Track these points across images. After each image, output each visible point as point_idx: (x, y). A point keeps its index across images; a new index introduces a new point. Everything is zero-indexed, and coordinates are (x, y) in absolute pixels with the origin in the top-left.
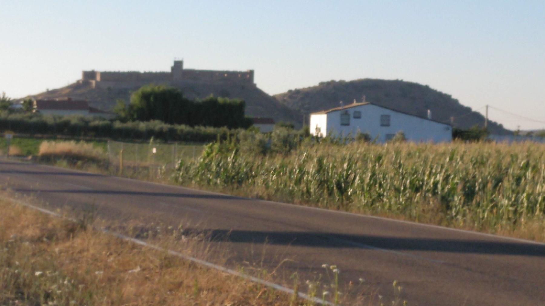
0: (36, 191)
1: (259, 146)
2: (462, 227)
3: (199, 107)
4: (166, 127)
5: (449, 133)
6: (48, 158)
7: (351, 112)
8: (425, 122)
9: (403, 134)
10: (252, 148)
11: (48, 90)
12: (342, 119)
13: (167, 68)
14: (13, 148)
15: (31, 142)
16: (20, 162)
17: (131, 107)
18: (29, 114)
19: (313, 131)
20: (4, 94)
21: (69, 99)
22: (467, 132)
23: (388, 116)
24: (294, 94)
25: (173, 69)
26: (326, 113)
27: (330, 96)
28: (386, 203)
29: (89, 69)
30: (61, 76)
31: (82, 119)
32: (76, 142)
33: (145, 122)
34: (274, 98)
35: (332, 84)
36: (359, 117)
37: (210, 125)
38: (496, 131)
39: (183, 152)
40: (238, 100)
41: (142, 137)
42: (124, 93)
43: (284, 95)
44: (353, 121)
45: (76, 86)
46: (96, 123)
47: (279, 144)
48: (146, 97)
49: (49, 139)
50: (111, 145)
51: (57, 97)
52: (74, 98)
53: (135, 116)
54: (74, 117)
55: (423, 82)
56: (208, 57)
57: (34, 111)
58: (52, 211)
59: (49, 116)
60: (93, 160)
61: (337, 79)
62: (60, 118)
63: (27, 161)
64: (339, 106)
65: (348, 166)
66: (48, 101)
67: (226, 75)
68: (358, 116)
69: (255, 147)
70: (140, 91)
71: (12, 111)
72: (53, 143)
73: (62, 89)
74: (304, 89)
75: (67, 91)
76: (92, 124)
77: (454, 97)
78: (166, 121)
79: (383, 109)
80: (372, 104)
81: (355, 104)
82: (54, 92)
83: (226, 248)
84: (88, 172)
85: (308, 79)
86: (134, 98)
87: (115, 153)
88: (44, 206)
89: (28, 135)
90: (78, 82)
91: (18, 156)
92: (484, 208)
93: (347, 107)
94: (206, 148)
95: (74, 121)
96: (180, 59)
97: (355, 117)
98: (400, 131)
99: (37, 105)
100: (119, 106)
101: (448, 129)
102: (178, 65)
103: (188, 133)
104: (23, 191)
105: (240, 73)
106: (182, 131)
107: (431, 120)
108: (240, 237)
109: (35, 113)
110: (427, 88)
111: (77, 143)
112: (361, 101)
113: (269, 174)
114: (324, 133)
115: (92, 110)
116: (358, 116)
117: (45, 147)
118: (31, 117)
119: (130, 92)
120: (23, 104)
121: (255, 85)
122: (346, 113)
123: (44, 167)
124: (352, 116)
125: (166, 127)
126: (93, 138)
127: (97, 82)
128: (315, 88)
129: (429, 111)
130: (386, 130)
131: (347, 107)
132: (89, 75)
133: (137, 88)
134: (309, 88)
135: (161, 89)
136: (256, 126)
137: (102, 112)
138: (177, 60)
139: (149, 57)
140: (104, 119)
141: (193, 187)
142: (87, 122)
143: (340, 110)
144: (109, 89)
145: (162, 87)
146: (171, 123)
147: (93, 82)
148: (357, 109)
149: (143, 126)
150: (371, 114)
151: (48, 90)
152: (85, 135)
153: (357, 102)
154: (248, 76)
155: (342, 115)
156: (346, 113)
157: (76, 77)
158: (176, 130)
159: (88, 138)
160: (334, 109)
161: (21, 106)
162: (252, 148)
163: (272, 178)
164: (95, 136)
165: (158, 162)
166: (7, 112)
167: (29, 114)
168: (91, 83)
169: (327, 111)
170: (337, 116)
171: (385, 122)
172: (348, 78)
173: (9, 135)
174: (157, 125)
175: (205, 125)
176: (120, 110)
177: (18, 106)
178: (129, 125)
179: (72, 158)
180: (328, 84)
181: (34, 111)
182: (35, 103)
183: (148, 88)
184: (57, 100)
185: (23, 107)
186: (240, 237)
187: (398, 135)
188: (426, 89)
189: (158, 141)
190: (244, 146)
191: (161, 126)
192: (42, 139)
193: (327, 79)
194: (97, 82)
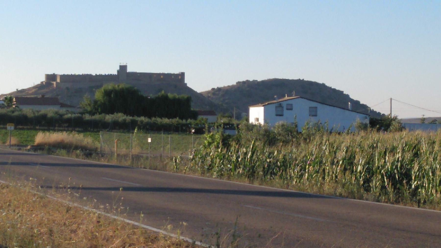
0: (79, 188)
2: (276, 185)
3: (153, 101)
6: (40, 147)
7: (284, 104)
11: (17, 90)
13: (114, 71)
14: (12, 138)
17: (96, 102)
19: (252, 120)
22: (381, 120)
26: (263, 106)
30: (29, 78)
31: (56, 113)
34: (201, 94)
35: (247, 83)
36: (291, 109)
39: (196, 143)
42: (91, 91)
43: (208, 92)
44: (286, 112)
48: (107, 93)
49: (44, 130)
50: (103, 135)
54: (50, 111)
55: (313, 80)
56: (147, 61)
58: (158, 227)
59: (28, 110)
61: (251, 80)
62: (38, 112)
64: (275, 99)
66: (21, 98)
68: (290, 108)
70: (102, 89)
72: (47, 134)
73: (29, 89)
74: (224, 87)
75: (34, 90)
76: (66, 117)
78: (126, 113)
79: (312, 102)
80: (302, 98)
81: (286, 98)
82: (23, 91)
86: (99, 95)
90: (42, 82)
93: (280, 100)
95: (50, 115)
96: (125, 64)
97: (287, 109)
100: (85, 101)
101: (366, 118)
102: (123, 68)
103: (147, 124)
105: (174, 75)
107: (351, 111)
110: (323, 85)
111: (69, 134)
114: (262, 122)
115: (63, 105)
116: (290, 108)
117: (41, 137)
118: (13, 112)
122: (280, 105)
125: (129, 118)
126: (66, 129)
127: (57, 83)
128: (233, 86)
129: (349, 103)
131: (280, 100)
132: (51, 78)
135: (120, 87)
138: (122, 64)
142: (61, 116)
143: (275, 103)
144: (67, 88)
146: (133, 116)
148: (290, 102)
149: (109, 118)
150: (301, 106)
154: (180, 77)
155: (276, 107)
157: (41, 79)
158: (137, 121)
160: (270, 102)
162: (258, 138)
164: (67, 127)
168: (53, 84)
169: (263, 105)
170: (273, 108)
172: (260, 78)
173: (10, 127)
174: (120, 117)
176: (86, 105)
178: (97, 117)
180: (244, 82)
182: (14, 100)
191: (123, 118)
194: (57, 83)
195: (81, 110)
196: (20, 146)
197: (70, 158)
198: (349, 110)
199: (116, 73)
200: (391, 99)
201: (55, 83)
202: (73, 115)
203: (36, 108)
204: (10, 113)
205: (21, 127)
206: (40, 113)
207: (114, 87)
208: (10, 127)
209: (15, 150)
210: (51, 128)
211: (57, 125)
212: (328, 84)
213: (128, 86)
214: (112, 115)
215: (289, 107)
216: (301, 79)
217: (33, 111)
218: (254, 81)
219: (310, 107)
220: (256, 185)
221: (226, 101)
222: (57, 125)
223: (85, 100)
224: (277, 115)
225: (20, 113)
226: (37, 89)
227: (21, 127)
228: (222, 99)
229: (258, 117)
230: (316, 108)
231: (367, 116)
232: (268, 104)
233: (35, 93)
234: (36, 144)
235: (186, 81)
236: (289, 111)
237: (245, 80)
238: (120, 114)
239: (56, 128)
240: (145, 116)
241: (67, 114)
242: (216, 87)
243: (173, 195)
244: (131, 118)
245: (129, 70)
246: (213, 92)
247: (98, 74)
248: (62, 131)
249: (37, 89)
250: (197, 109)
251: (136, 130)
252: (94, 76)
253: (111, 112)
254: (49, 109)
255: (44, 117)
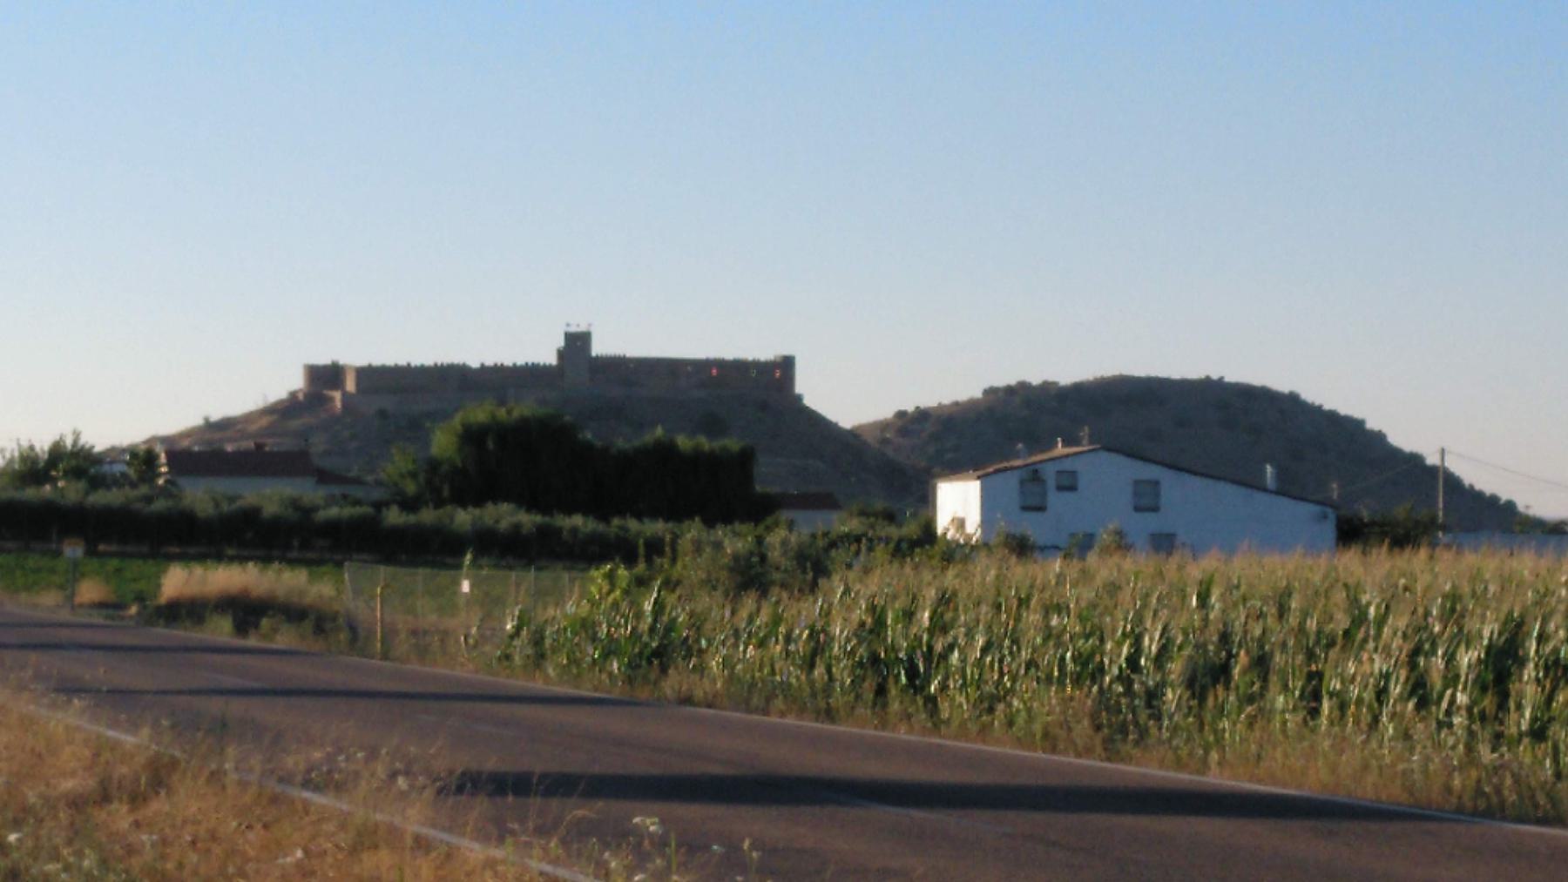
0: (99, 691)
1: (731, 570)
4: (528, 520)
5: (1329, 530)
6: (187, 611)
7: (1049, 473)
8: (1259, 496)
9: (1119, 534)
10: (714, 576)
11: (206, 419)
12: (1022, 493)
15: (135, 567)
16: (101, 621)
17: (433, 466)
18: (144, 490)
19: (943, 522)
20: (77, 435)
21: (259, 447)
23: (1156, 483)
24: (912, 423)
25: (561, 354)
27: (1005, 430)
28: (1018, 711)
29: (323, 359)
31: (295, 504)
32: (260, 565)
33: (470, 509)
34: (854, 434)
35: (1020, 392)
36: (1072, 488)
37: (654, 514)
38: (1489, 518)
40: (733, 444)
41: (434, 550)
42: (415, 429)
43: (883, 426)
44: (1055, 499)
45: (287, 409)
46: (334, 512)
47: (785, 563)
48: (472, 437)
49: (184, 558)
51: (230, 440)
52: (271, 445)
53: (446, 493)
54: (269, 496)
55: (1280, 383)
56: (662, 318)
57: (161, 482)
59: (200, 496)
60: (294, 613)
61: (1035, 380)
62: (232, 499)
63: (122, 618)
65: (931, 619)
66: (207, 453)
67: (714, 372)
68: (1068, 484)
69: (724, 575)
70: (457, 421)
71: (97, 482)
72: (198, 570)
73: (248, 418)
74: (941, 407)
75: (264, 421)
77: (1372, 424)
78: (532, 505)
79: (1140, 464)
80: (1109, 450)
81: (1060, 449)
82: (226, 424)
83: (481, 806)
84: (274, 646)
85: (953, 381)
86: (443, 442)
87: (356, 591)
88: (115, 724)
89: (145, 549)
90: (293, 395)
91: (102, 605)
92: (1234, 716)
94: (598, 574)
95: (270, 509)
96: (583, 328)
97: (1060, 488)
98: (1111, 527)
99: (169, 463)
100: (398, 464)
101: (1325, 517)
102: (577, 343)
103: (594, 538)
104: (69, 689)
105: (756, 365)
106: (574, 531)
107: (1278, 493)
108: (510, 785)
109: (162, 488)
110: (1293, 398)
112: (1077, 442)
113: (740, 642)
115: (323, 477)
116: (1068, 484)
117: (176, 581)
118: (149, 499)
119: (428, 425)
120: (128, 464)
121: (799, 398)
122: (1034, 476)
123: (162, 633)
124: (1051, 483)
125: (528, 520)
127: (345, 394)
128: (971, 405)
129: (1269, 468)
130: (1151, 522)
132: (324, 377)
133: (446, 416)
134: (957, 404)
135: (516, 414)
136: (784, 515)
137: (358, 481)
138: (573, 329)
139: (489, 317)
140: (357, 502)
141: (550, 679)
142: (307, 512)
144: (382, 414)
145: (525, 408)
146: (545, 510)
147: (337, 395)
148: (1067, 465)
149: (463, 518)
150: (1107, 477)
151: (206, 419)
152: (305, 545)
153: (1066, 443)
155: (1022, 482)
156: (1034, 476)
157: (288, 382)
158: (559, 530)
159: (310, 555)
161: (124, 468)
163: (745, 651)
165: (472, 617)
166: (82, 485)
167: (144, 490)
168: (332, 399)
169: (980, 473)
170: (1011, 482)
171: (1146, 499)
172: (1067, 375)
174: (505, 515)
175: (639, 516)
176: (402, 476)
177: (118, 468)
178: (428, 516)
179: (247, 611)
180: (1010, 391)
181: (161, 482)
182: (163, 458)
183: (480, 414)
184: (229, 448)
185: (131, 472)
186: (510, 785)
187: (1104, 537)
188: (1289, 406)
189: (484, 561)
190: (690, 568)
191: (514, 519)
192: (172, 558)
193: (1006, 377)
194: (345, 394)
195: (377, 494)
196: (111, 607)
197: (428, 669)
198: (1265, 490)
199: (550, 359)
200: (1443, 451)
201: (337, 395)
202: (348, 512)
203: (223, 486)
204: (138, 506)
205: (177, 550)
206: (239, 504)
207: (494, 417)
208: (73, 550)
209: (97, 618)
210: (276, 553)
211: (296, 543)
212: (1312, 394)
213: (541, 411)
214: (477, 512)
215: (1066, 483)
216: (1215, 377)
217: (214, 499)
218: (1046, 387)
219: (1137, 483)
220: (1146, 768)
221: (949, 456)
222: (296, 543)
223: (396, 458)
224: (1025, 508)
225: (170, 503)
226: (275, 417)
227: (177, 550)
228: (931, 450)
229: (960, 514)
230: (1156, 483)
231: (1329, 510)
232: (997, 471)
233: (269, 431)
234: (163, 600)
235: (801, 386)
236: (1067, 495)
237: (1013, 382)
238: (505, 507)
239: (294, 554)
240: (585, 514)
241: (328, 505)
242: (910, 408)
243: (281, 702)
244: (538, 519)
245: (599, 348)
246: (900, 423)
247: (489, 362)
248: (242, 559)
249: (275, 417)
250: (773, 489)
251: (469, 556)
252: (476, 371)
253: (477, 498)
254: (268, 491)
255: (250, 517)
